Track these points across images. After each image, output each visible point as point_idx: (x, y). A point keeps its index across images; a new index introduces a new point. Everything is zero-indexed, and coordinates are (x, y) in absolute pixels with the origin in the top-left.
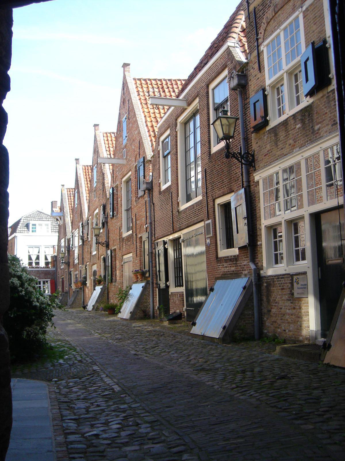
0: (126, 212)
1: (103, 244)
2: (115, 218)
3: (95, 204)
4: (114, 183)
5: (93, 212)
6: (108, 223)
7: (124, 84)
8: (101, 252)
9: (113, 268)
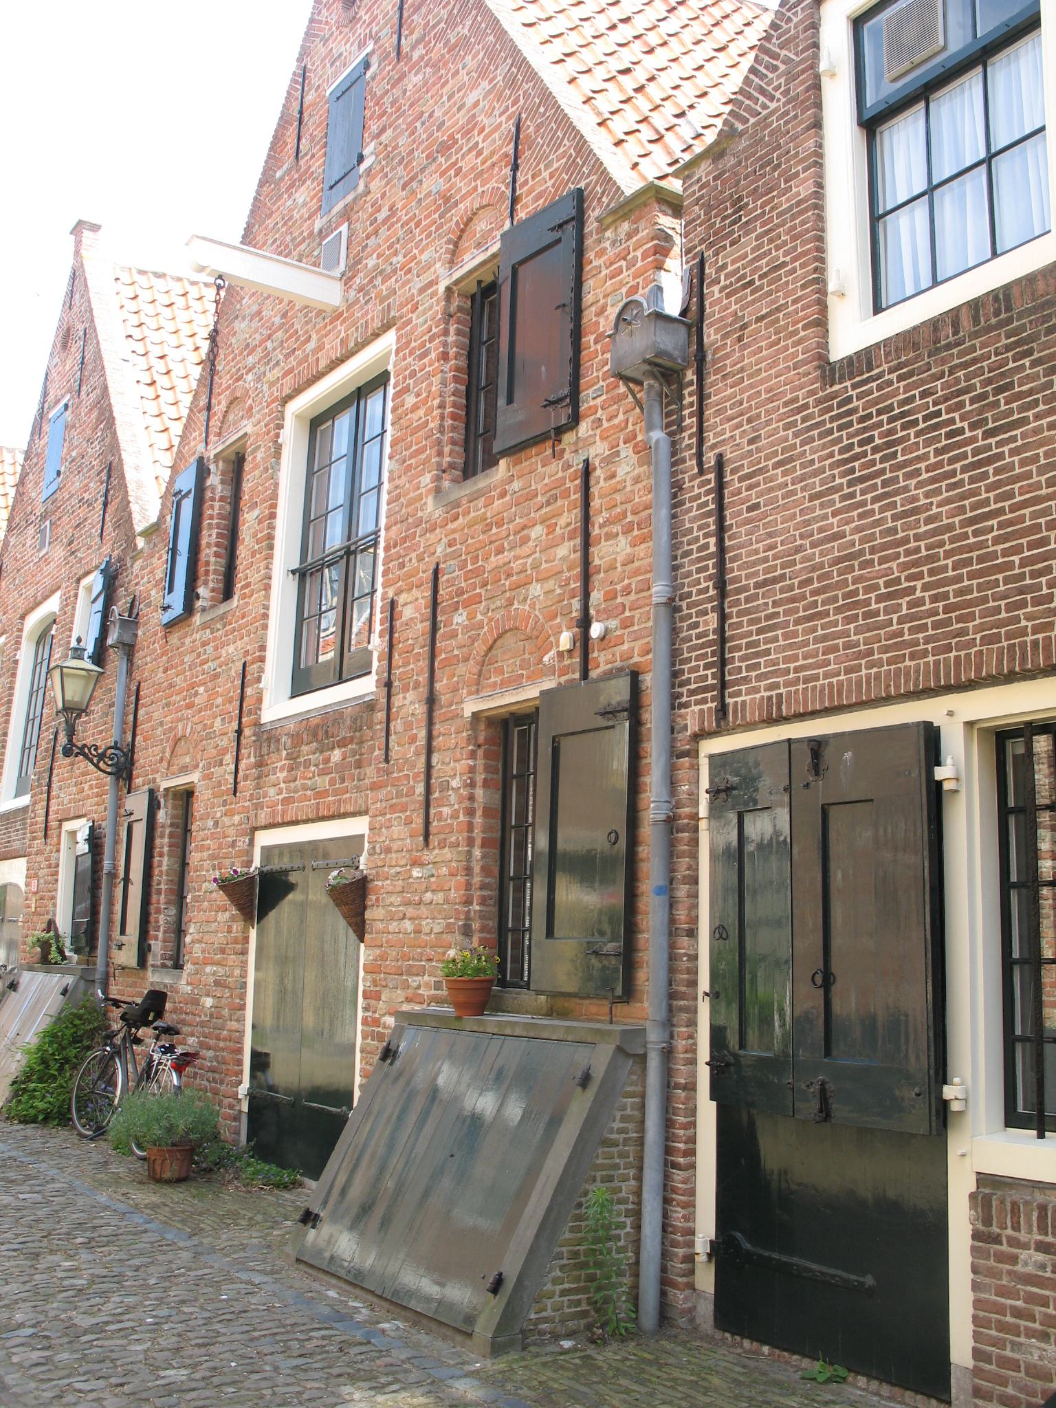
0: (293, 584)
1: (102, 757)
2: (197, 619)
3: (39, 577)
4: (212, 438)
5: (23, 617)
6: (139, 655)
7: (74, 277)
8: (63, 796)
9: (159, 892)
